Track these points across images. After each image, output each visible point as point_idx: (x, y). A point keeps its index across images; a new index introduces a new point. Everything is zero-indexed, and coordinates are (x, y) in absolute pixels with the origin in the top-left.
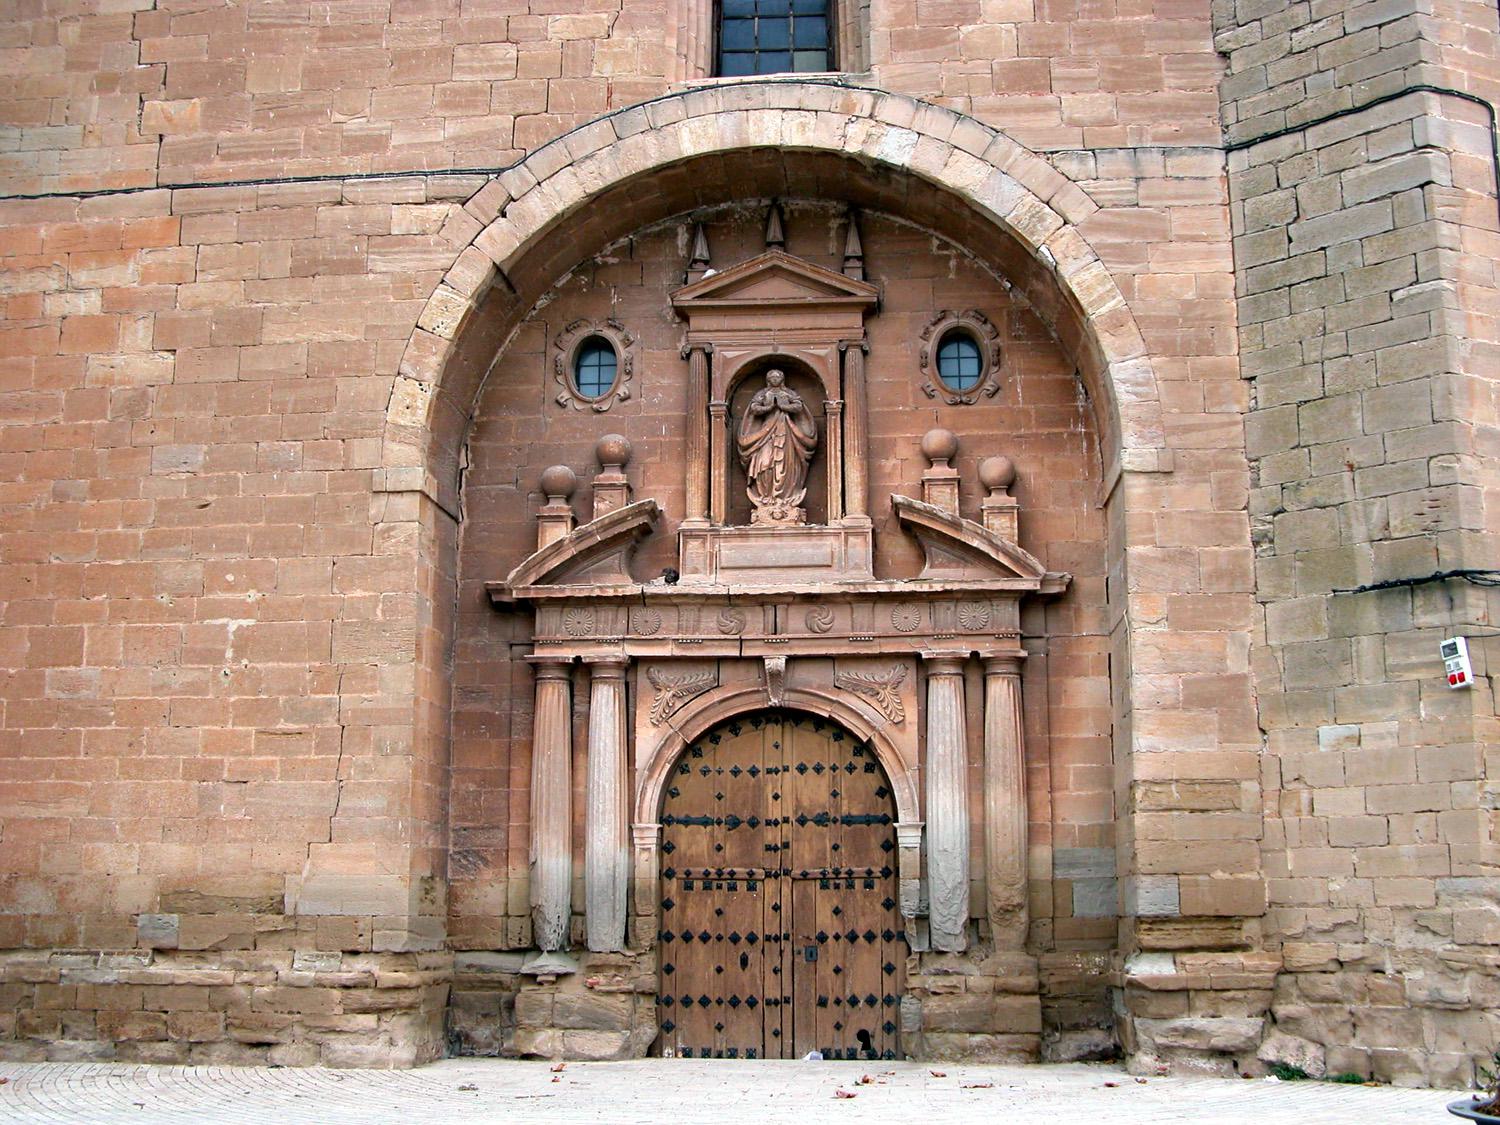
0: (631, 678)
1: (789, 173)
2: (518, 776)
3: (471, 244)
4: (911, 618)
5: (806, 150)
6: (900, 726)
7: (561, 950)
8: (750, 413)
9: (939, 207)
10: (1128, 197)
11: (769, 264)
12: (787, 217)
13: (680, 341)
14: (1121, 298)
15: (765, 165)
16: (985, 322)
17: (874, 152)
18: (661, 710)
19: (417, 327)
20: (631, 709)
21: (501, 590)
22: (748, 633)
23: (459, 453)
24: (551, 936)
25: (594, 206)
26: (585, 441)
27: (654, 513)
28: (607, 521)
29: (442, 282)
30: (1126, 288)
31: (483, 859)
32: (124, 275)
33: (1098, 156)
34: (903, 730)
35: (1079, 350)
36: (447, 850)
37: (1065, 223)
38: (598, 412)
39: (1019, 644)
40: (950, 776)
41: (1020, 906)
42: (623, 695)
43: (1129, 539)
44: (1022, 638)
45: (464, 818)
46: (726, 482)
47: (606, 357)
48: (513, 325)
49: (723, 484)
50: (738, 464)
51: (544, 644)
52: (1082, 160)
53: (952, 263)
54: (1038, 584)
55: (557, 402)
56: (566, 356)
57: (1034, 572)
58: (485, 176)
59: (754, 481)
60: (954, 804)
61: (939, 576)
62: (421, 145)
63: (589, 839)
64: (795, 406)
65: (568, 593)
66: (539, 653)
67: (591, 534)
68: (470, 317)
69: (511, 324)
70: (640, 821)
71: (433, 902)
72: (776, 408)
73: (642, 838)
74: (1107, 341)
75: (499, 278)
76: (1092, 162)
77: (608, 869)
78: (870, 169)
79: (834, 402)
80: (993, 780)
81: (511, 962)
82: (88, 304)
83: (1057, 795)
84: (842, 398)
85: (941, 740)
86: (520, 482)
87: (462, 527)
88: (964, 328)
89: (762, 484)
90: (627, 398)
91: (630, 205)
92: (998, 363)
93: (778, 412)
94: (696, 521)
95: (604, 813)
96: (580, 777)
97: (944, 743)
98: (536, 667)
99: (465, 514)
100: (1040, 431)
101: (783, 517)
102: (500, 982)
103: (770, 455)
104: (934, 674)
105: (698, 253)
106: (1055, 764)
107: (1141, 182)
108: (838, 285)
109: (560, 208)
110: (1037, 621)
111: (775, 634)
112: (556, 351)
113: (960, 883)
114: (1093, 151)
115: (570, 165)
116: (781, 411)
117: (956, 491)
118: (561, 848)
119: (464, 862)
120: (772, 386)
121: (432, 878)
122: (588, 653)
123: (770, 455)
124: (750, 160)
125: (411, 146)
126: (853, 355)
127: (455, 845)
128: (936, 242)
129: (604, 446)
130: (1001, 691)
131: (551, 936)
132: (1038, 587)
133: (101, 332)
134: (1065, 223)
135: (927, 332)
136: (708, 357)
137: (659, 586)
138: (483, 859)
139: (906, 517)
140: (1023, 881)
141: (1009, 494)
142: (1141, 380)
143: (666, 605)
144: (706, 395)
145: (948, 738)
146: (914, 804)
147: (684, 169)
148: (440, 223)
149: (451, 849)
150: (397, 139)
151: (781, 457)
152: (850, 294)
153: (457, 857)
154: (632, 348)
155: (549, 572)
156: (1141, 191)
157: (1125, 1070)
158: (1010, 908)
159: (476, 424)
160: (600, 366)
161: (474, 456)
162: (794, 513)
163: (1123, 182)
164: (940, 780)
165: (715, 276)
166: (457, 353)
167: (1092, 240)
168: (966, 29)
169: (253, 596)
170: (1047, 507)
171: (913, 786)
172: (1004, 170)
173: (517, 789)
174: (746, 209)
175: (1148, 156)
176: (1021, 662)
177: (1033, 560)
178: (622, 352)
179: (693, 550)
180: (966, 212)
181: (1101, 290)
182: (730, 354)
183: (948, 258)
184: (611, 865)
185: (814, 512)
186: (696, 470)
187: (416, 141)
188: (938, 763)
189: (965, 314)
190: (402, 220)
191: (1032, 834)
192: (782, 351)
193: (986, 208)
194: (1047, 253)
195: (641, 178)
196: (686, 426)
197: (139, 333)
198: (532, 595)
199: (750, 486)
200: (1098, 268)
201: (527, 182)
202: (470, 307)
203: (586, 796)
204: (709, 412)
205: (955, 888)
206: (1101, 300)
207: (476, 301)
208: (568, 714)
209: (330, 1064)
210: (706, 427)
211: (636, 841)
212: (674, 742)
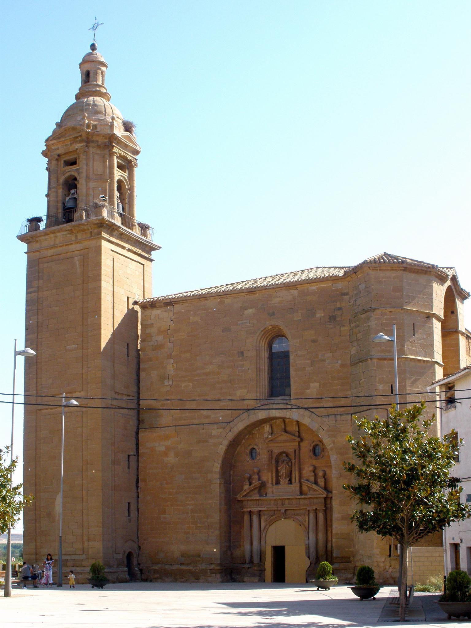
7: (249, 563)
24: (247, 561)
30: (334, 442)
32: (168, 443)
50: (277, 471)
74: (330, 452)
79: (293, 461)
82: (163, 449)
103: (283, 471)
122: (252, 510)
123: (283, 471)
131: (247, 561)
133: (166, 454)
150: (213, 416)
168: (308, 391)
169: (193, 502)
179: (270, 490)
190: (214, 433)
197: (172, 454)
200: (329, 439)
209: (208, 582)
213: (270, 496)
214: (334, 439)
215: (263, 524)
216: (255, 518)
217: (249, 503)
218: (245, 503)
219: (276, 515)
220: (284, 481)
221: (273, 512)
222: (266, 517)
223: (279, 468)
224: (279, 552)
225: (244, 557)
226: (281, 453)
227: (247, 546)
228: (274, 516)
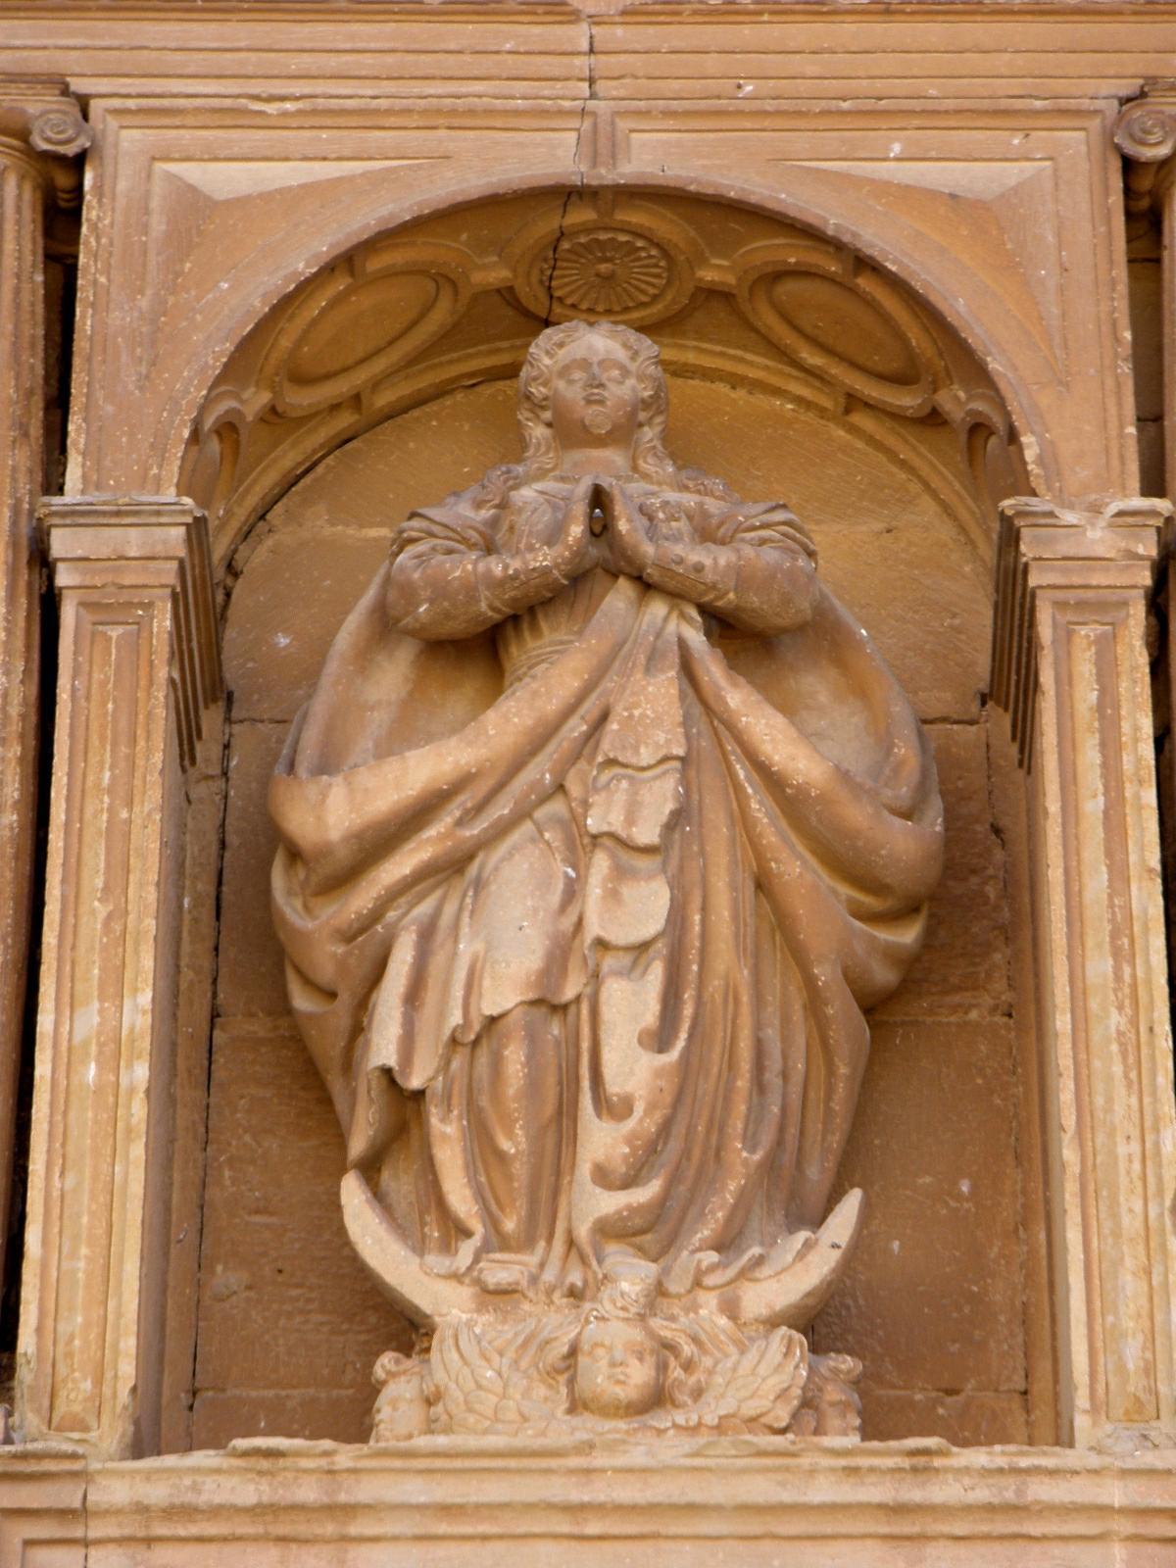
8: (386, 626)
49: (138, 1111)
59: (406, 1106)
72: (605, 561)
101: (658, 1398)
116: (646, 586)
120: (570, 433)
151: (644, 909)
162: (774, 1370)
192: (650, 155)
199: (370, 1169)
204: (41, 559)
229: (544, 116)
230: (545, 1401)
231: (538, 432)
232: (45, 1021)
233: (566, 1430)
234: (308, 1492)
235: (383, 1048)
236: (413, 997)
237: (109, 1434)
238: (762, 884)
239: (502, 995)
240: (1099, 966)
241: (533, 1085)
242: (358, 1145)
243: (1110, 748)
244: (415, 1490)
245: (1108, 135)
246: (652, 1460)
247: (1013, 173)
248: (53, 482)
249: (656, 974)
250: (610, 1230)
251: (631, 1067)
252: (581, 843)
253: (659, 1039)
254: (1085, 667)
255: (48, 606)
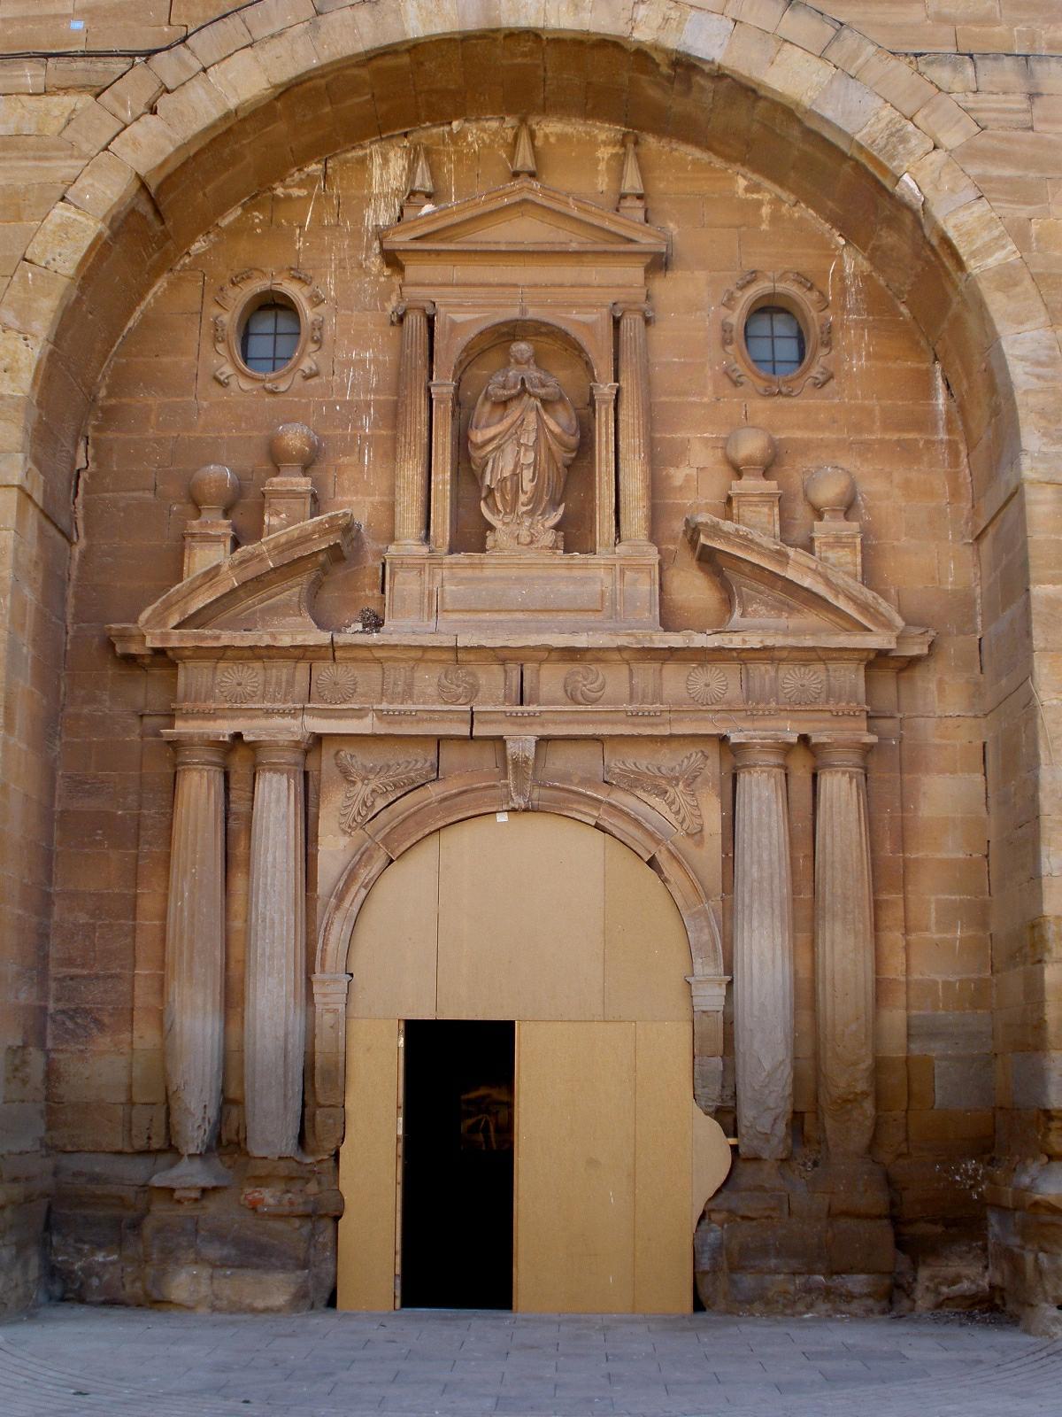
0: (312, 765)
1: (550, 74)
2: (149, 904)
3: (106, 149)
4: (719, 682)
5: (579, 37)
6: (696, 837)
9: (755, 127)
10: (1021, 116)
11: (517, 198)
12: (539, 143)
13: (389, 299)
14: (1014, 247)
15: (519, 60)
16: (810, 289)
17: (672, 42)
18: (355, 810)
19: (26, 260)
20: (312, 810)
21: (125, 636)
22: (484, 703)
23: (76, 445)
24: (194, 1131)
25: (279, 105)
26: (255, 433)
27: (349, 529)
28: (283, 540)
29: (63, 199)
30: (1020, 234)
31: (96, 1021)
33: (979, 63)
34: (700, 843)
35: (945, 325)
36: (46, 1008)
37: (935, 147)
38: (273, 393)
39: (864, 725)
40: (768, 909)
41: (865, 1094)
42: (301, 789)
43: (1033, 574)
44: (869, 718)
45: (70, 962)
46: (452, 490)
47: (284, 324)
48: (158, 276)
51: (188, 715)
52: (956, 68)
53: (765, 211)
54: (894, 640)
55: (216, 379)
56: (229, 318)
57: (888, 625)
58: (129, 60)
60: (774, 949)
61: (757, 626)
62: (39, 19)
63: (250, 995)
64: (550, 390)
65: (224, 641)
66: (182, 727)
67: (258, 557)
68: (100, 251)
69: (156, 272)
70: (323, 971)
71: (24, 1082)
73: (325, 995)
74: (997, 303)
75: (143, 197)
76: (970, 70)
77: (277, 1038)
78: (665, 69)
79: (605, 389)
80: (828, 917)
81: (136, 1170)
83: (913, 937)
84: (616, 380)
85: (755, 859)
86: (160, 487)
87: (77, 551)
88: (780, 295)
89: (503, 496)
90: (315, 374)
91: (327, 109)
92: (827, 344)
93: (526, 398)
94: (408, 543)
95: (271, 957)
96: (238, 905)
97: (760, 863)
98: (175, 745)
99: (82, 533)
100: (887, 437)
101: (532, 542)
102: (121, 1198)
103: (516, 450)
104: (745, 766)
105: (417, 183)
106: (911, 897)
107: (1036, 100)
108: (613, 228)
109: (232, 103)
110: (887, 689)
111: (522, 704)
112: (216, 310)
113: (782, 1062)
114: (971, 56)
115: (250, 45)
117: (776, 510)
118: (209, 1007)
119: (70, 1025)
120: (518, 362)
121: (24, 1047)
122: (252, 729)
124: (498, 51)
125: (25, 19)
126: (631, 325)
127: (58, 1000)
128: (742, 183)
129: (281, 437)
130: (839, 788)
131: (194, 1131)
132: (893, 646)
134: (935, 147)
135: (731, 298)
136: (430, 321)
137: (353, 634)
138: (96, 1021)
139: (709, 543)
140: (869, 1061)
141: (847, 519)
142: (1043, 358)
143: (364, 660)
144: (425, 373)
145: (765, 856)
146: (715, 951)
147: (406, 59)
148: (63, 121)
149: (52, 1006)
152: (631, 241)
153: (59, 1017)
154: (322, 309)
155: (199, 612)
156: (1037, 112)
157: (1027, 1331)
158: (851, 1097)
159: (101, 408)
160: (276, 334)
161: (96, 453)
162: (549, 538)
163: (1012, 97)
164: (755, 916)
165: (434, 212)
166: (78, 301)
167: (975, 169)
170: (898, 540)
171: (713, 923)
172: (852, 72)
173: (148, 923)
174: (484, 130)
175: (1045, 66)
176: (867, 750)
177: (884, 606)
178: (308, 313)
179: (406, 585)
180: (795, 132)
181: (986, 236)
182: (459, 317)
183: (759, 204)
184: (281, 1033)
185: (575, 535)
186: (411, 472)
187: (31, 13)
188: (751, 891)
189: (783, 277)
191: (880, 990)
192: (532, 313)
193: (827, 122)
194: (913, 185)
195: (348, 67)
196: (394, 415)
198: (174, 643)
199: (485, 499)
200: (981, 208)
201: (189, 68)
202: (99, 236)
203: (247, 932)
205: (775, 1069)
206: (987, 250)
207: (110, 227)
208: (221, 816)
210: (424, 416)
211: (317, 998)
212: (371, 857)
213: (400, 629)
214: (1023, 212)
215: (334, 848)
216: (274, 798)
217: (232, 676)
218: (190, 677)
219: (460, 771)
220: (523, 535)
221: (421, 760)
222: (362, 790)
223: (478, 436)
224: (461, 1070)
225: (168, 1103)
226: (505, 334)
227: (197, 1025)
228: (434, 791)
229: (513, 306)
230: (513, 543)
231: (512, 360)
232: (433, 478)
233: (517, 547)
234: (477, 561)
235: (487, 482)
236: (492, 471)
237: (445, 549)
238: (549, 449)
239: (507, 474)
240: (604, 468)
241: (512, 488)
242: (483, 495)
243: (607, 429)
244: (493, 561)
245: (611, 310)
246: (530, 556)
247: (594, 317)
248: (431, 378)
249: (532, 470)
250: (524, 513)
251: (528, 486)
252: (519, 445)
253: (532, 480)
254: (603, 414)
255: (431, 401)
